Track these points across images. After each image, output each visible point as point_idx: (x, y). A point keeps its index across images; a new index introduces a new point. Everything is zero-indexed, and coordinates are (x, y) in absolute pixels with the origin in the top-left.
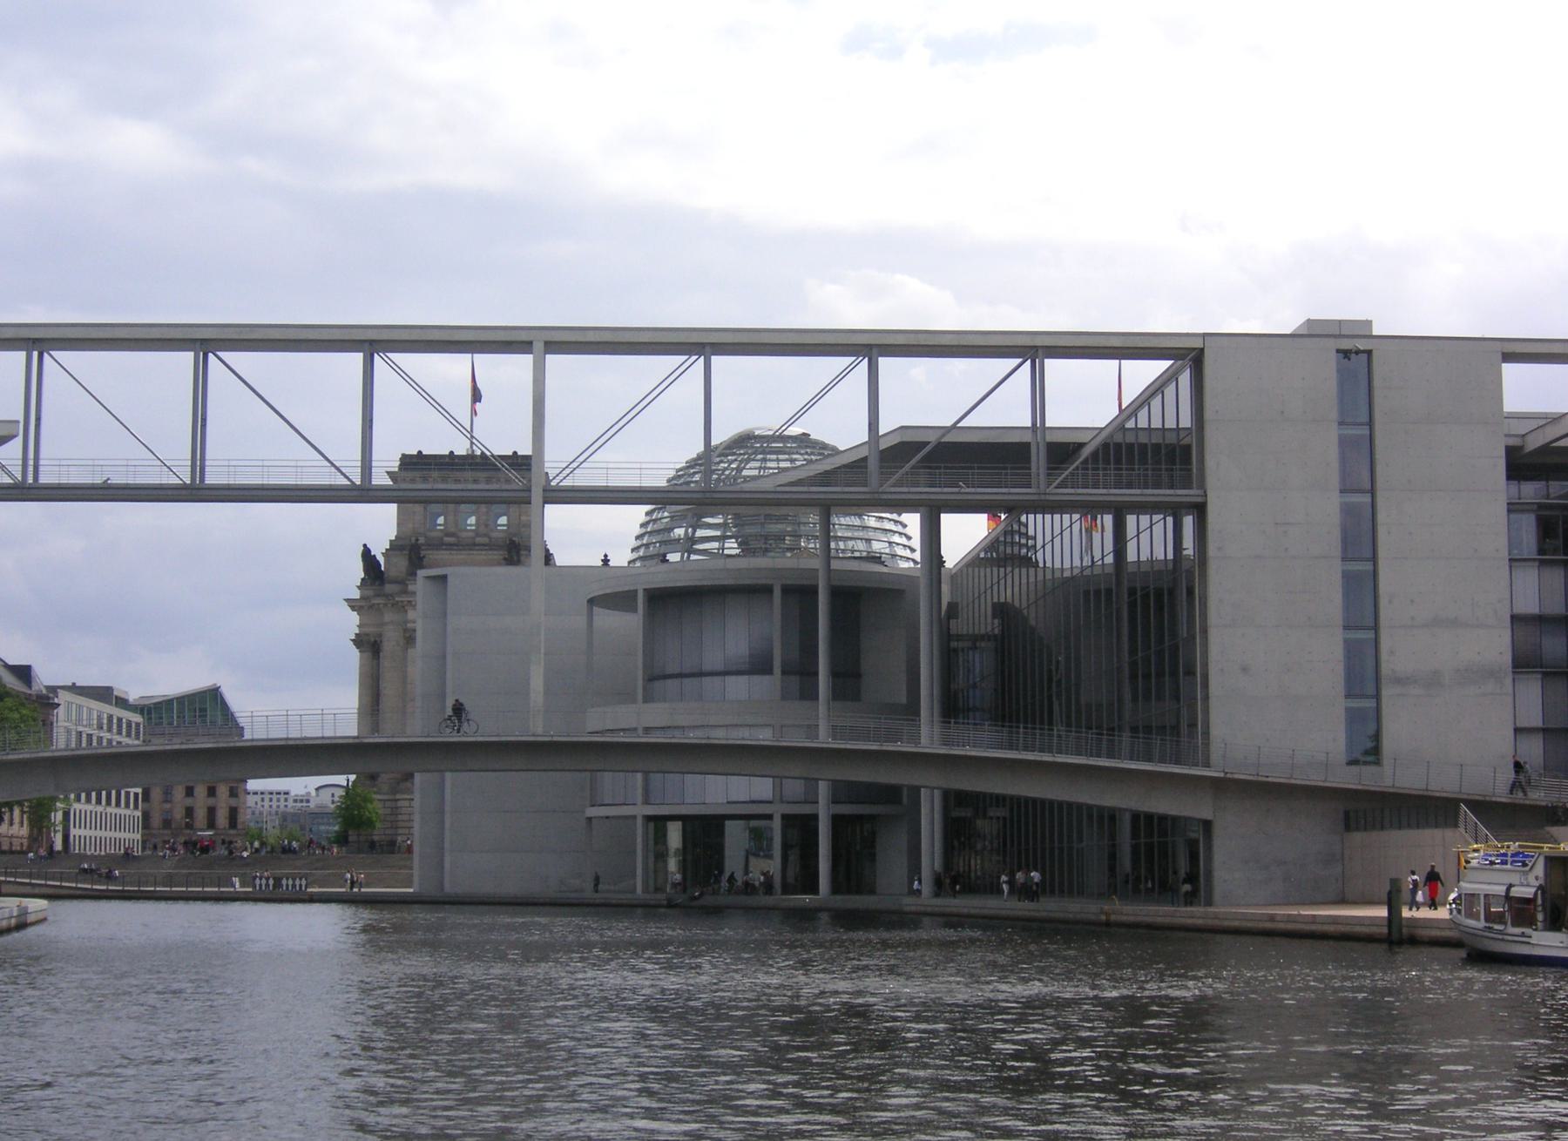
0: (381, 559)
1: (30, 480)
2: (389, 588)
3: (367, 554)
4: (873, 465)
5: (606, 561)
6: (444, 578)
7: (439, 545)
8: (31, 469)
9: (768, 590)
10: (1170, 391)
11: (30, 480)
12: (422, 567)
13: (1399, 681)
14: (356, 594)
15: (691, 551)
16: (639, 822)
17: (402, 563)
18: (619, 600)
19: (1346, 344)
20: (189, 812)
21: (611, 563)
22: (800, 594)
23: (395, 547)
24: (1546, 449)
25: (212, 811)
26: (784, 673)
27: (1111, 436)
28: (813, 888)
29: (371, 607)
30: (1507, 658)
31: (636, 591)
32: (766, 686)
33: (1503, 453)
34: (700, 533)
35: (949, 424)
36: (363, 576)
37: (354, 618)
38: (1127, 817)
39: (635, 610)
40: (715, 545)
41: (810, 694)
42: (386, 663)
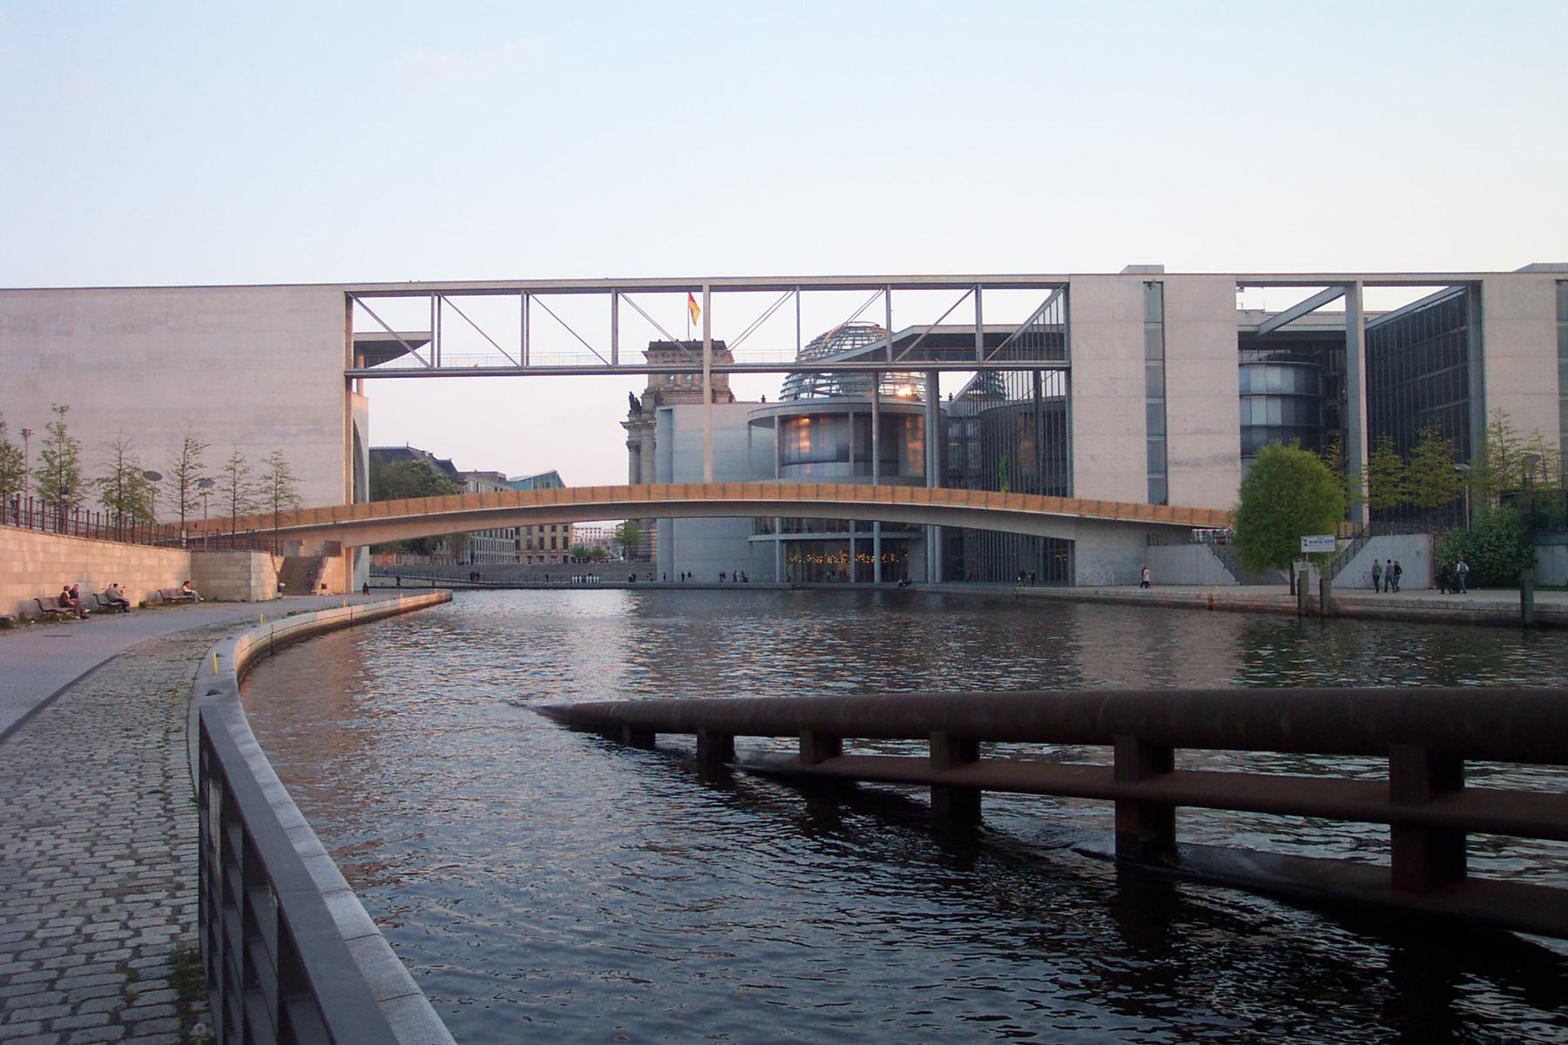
0: (640, 400)
1: (436, 366)
2: (645, 416)
3: (632, 397)
4: (889, 351)
5: (763, 399)
6: (671, 410)
7: (671, 391)
8: (436, 357)
9: (844, 416)
10: (1054, 305)
11: (436, 366)
12: (662, 405)
13: (1177, 464)
14: (627, 420)
15: (814, 392)
16: (778, 542)
17: (650, 402)
18: (766, 422)
19: (1149, 279)
20: (542, 540)
21: (767, 401)
22: (863, 417)
23: (647, 393)
24: (1271, 333)
25: (554, 539)
26: (855, 462)
27: (1027, 329)
28: (872, 579)
29: (635, 427)
30: (1238, 451)
31: (773, 417)
32: (844, 468)
33: (1236, 337)
34: (820, 382)
35: (933, 323)
36: (629, 409)
37: (626, 432)
38: (1042, 542)
39: (773, 427)
40: (828, 388)
41: (869, 472)
42: (644, 457)
